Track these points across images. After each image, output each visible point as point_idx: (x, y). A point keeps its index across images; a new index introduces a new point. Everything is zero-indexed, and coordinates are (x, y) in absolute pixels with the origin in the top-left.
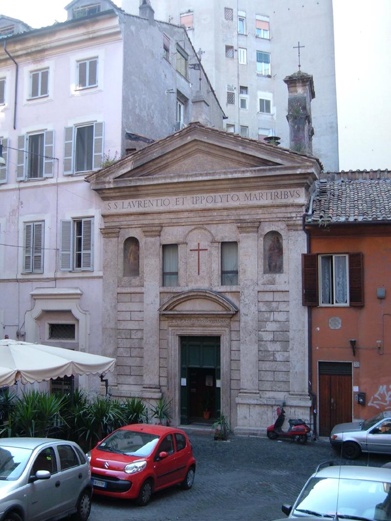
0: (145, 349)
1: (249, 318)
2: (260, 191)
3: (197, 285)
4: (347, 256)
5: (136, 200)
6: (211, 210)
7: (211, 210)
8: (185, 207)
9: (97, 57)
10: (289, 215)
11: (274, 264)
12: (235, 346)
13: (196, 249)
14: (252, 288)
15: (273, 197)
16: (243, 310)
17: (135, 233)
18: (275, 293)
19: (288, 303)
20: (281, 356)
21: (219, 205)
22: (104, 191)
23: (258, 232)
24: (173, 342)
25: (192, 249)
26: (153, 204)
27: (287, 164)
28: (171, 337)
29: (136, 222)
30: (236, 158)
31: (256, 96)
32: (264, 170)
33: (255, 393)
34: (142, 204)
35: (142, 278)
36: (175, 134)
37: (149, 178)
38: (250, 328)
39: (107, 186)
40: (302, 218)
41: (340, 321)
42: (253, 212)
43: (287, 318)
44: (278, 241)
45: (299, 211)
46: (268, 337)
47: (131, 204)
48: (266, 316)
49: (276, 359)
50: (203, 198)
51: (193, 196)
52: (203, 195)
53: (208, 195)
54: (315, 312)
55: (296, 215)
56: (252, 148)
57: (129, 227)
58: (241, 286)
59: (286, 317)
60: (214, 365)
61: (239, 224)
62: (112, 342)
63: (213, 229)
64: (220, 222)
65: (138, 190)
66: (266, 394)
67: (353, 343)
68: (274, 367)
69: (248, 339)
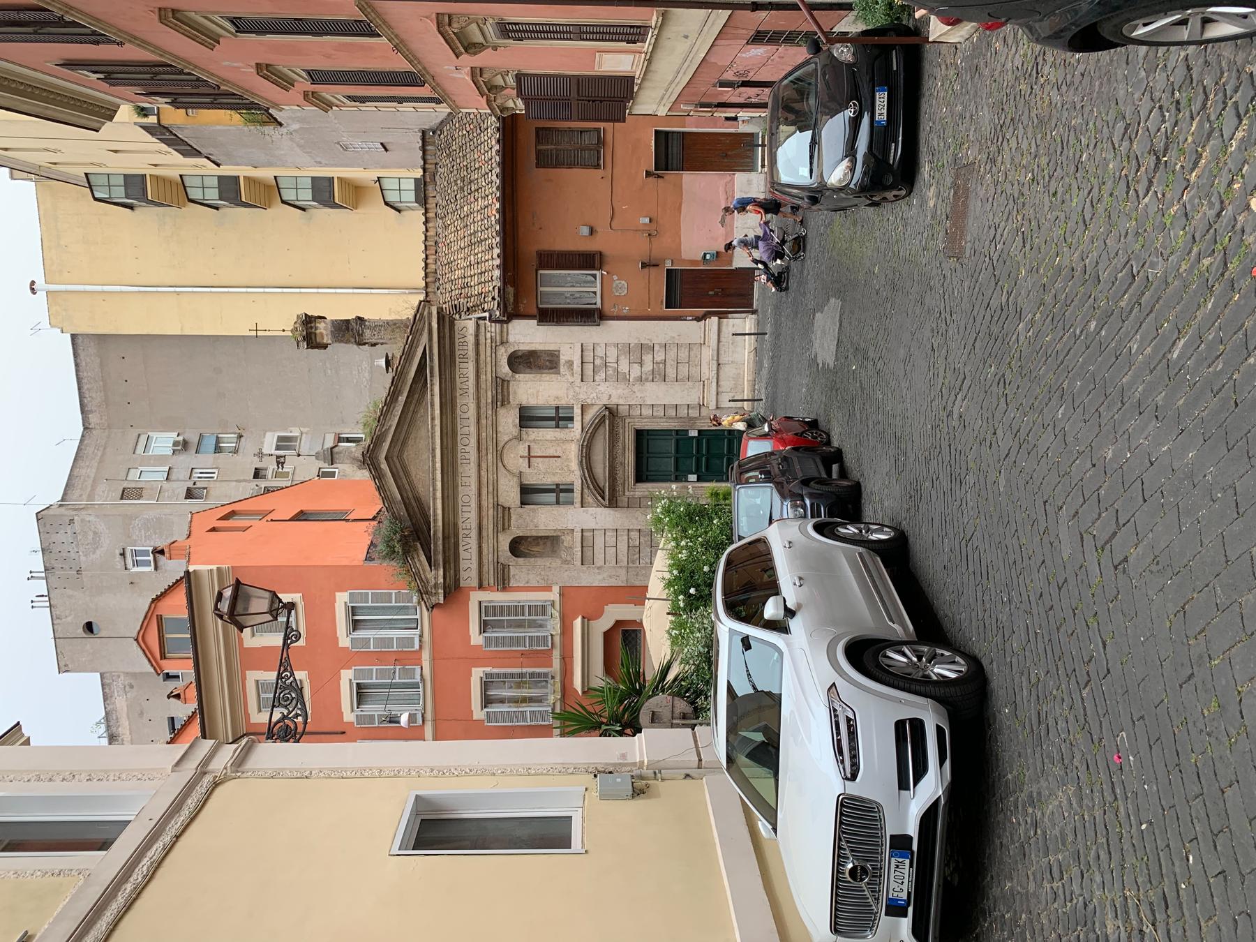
1: (615, 393)
12: (647, 412)
17: (505, 541)
21: (473, 429)
26: (468, 518)
29: (491, 541)
42: (483, 386)
54: (609, 309)
57: (496, 550)
63: (503, 438)
67: (644, 265)
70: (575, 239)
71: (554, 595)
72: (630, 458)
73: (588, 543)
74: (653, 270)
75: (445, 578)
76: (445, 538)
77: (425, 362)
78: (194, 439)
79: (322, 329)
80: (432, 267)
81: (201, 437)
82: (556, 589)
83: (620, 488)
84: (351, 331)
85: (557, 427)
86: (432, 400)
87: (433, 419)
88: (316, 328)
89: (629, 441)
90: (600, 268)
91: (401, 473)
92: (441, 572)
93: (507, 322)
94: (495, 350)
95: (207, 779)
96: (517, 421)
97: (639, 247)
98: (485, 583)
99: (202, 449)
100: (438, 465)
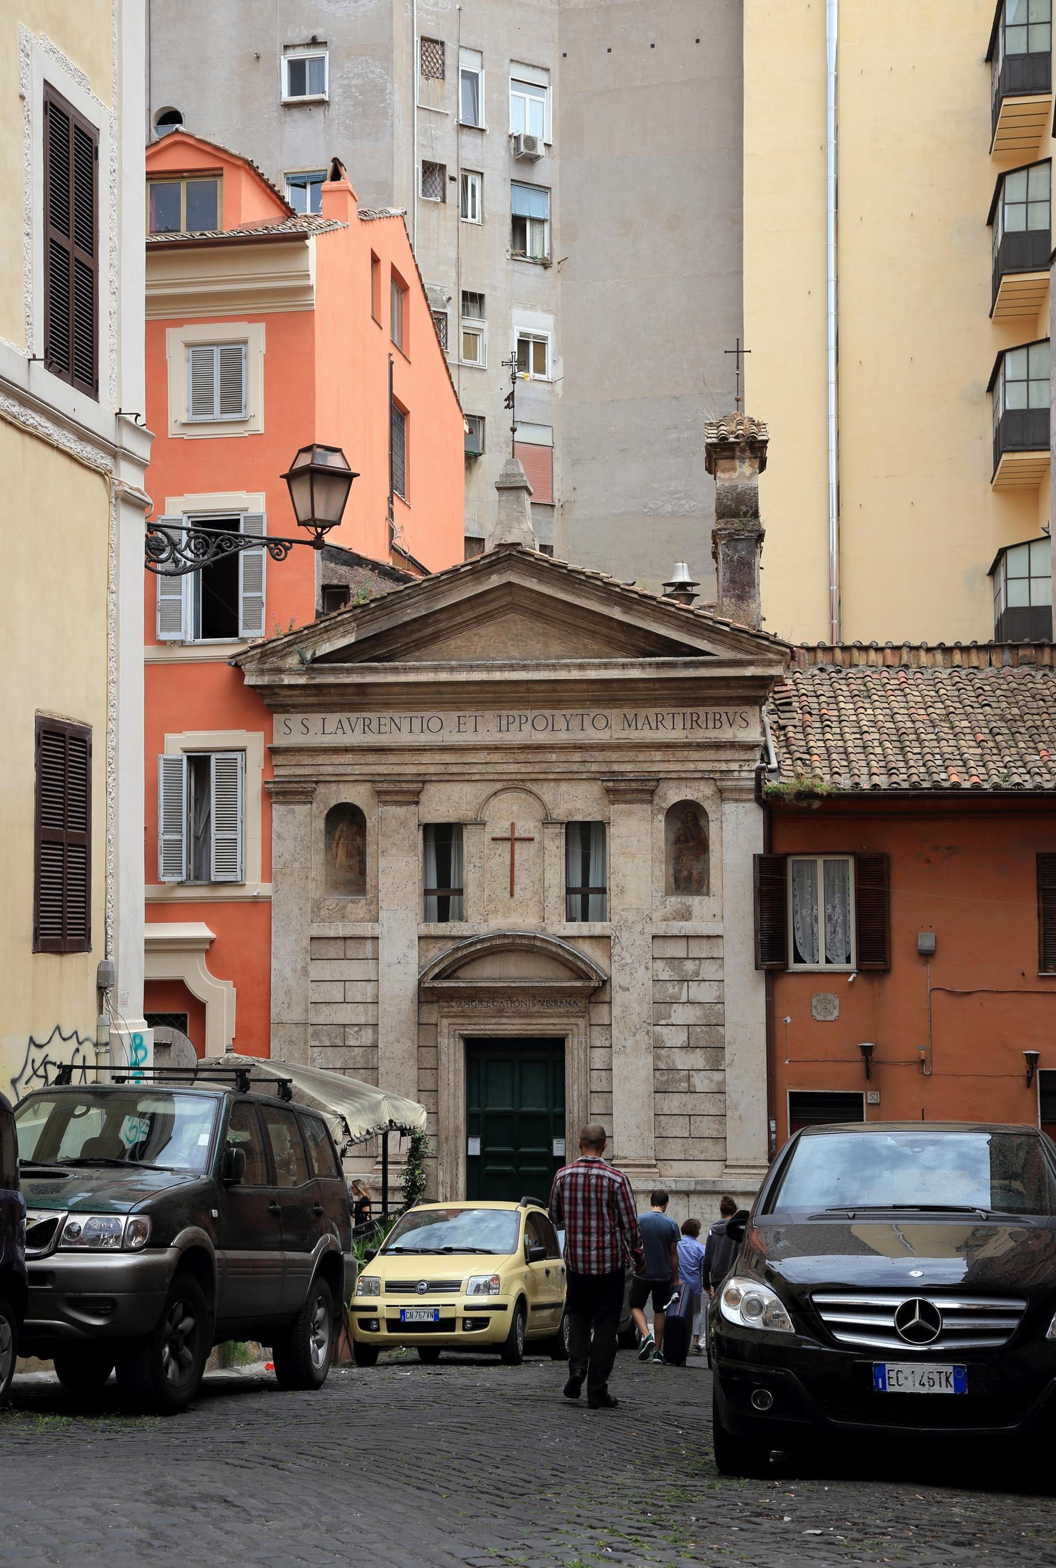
0: (382, 1070)
1: (631, 997)
2: (658, 710)
3: (510, 920)
4: (851, 862)
5: (357, 715)
6: (545, 748)
7: (545, 748)
8: (480, 737)
9: (245, 342)
10: (724, 767)
11: (685, 873)
12: (598, 1058)
13: (505, 835)
14: (639, 928)
15: (688, 725)
16: (618, 979)
17: (356, 795)
18: (691, 942)
19: (720, 961)
20: (706, 1082)
21: (562, 737)
22: (277, 690)
23: (651, 802)
24: (452, 1052)
25: (495, 836)
26: (401, 729)
27: (724, 653)
28: (446, 1041)
29: (357, 770)
30: (605, 631)
31: (508, 325)
32: (672, 665)
33: (649, 1166)
34: (374, 725)
35: (375, 901)
36: (463, 566)
37: (397, 668)
38: (635, 1019)
39: (287, 680)
40: (753, 775)
41: (837, 1002)
42: (641, 757)
43: (719, 996)
44: (697, 825)
45: (746, 757)
46: (677, 1037)
47: (346, 725)
48: (671, 990)
49: (694, 1086)
50: (524, 719)
51: (499, 713)
52: (524, 712)
53: (535, 712)
54: (787, 985)
55: (741, 766)
56: (645, 613)
57: (339, 780)
58: (614, 923)
59: (716, 994)
60: (547, 1107)
61: (611, 784)
62: (296, 1055)
63: (547, 792)
64: (564, 776)
65: (366, 694)
66: (671, 1167)
67: (867, 1051)
68: (690, 1106)
69: (629, 1043)
70: (912, 922)
71: (255, 886)
72: (511, 1026)
73: (352, 949)
74: (858, 1068)
75: (290, 687)
76: (361, 688)
77: (688, 655)
78: (541, 174)
79: (739, 474)
80: (858, 657)
81: (545, 189)
82: (264, 889)
83: (455, 1007)
84: (739, 529)
85: (570, 891)
86: (615, 666)
87: (581, 667)
88: (742, 460)
89: (543, 1024)
90: (860, 970)
91: (482, 610)
92: (302, 681)
93: (758, 800)
94: (706, 777)
95: (103, 460)
96: (579, 818)
97: (900, 1042)
98: (278, 760)
99: (521, 192)
100: (497, 676)
